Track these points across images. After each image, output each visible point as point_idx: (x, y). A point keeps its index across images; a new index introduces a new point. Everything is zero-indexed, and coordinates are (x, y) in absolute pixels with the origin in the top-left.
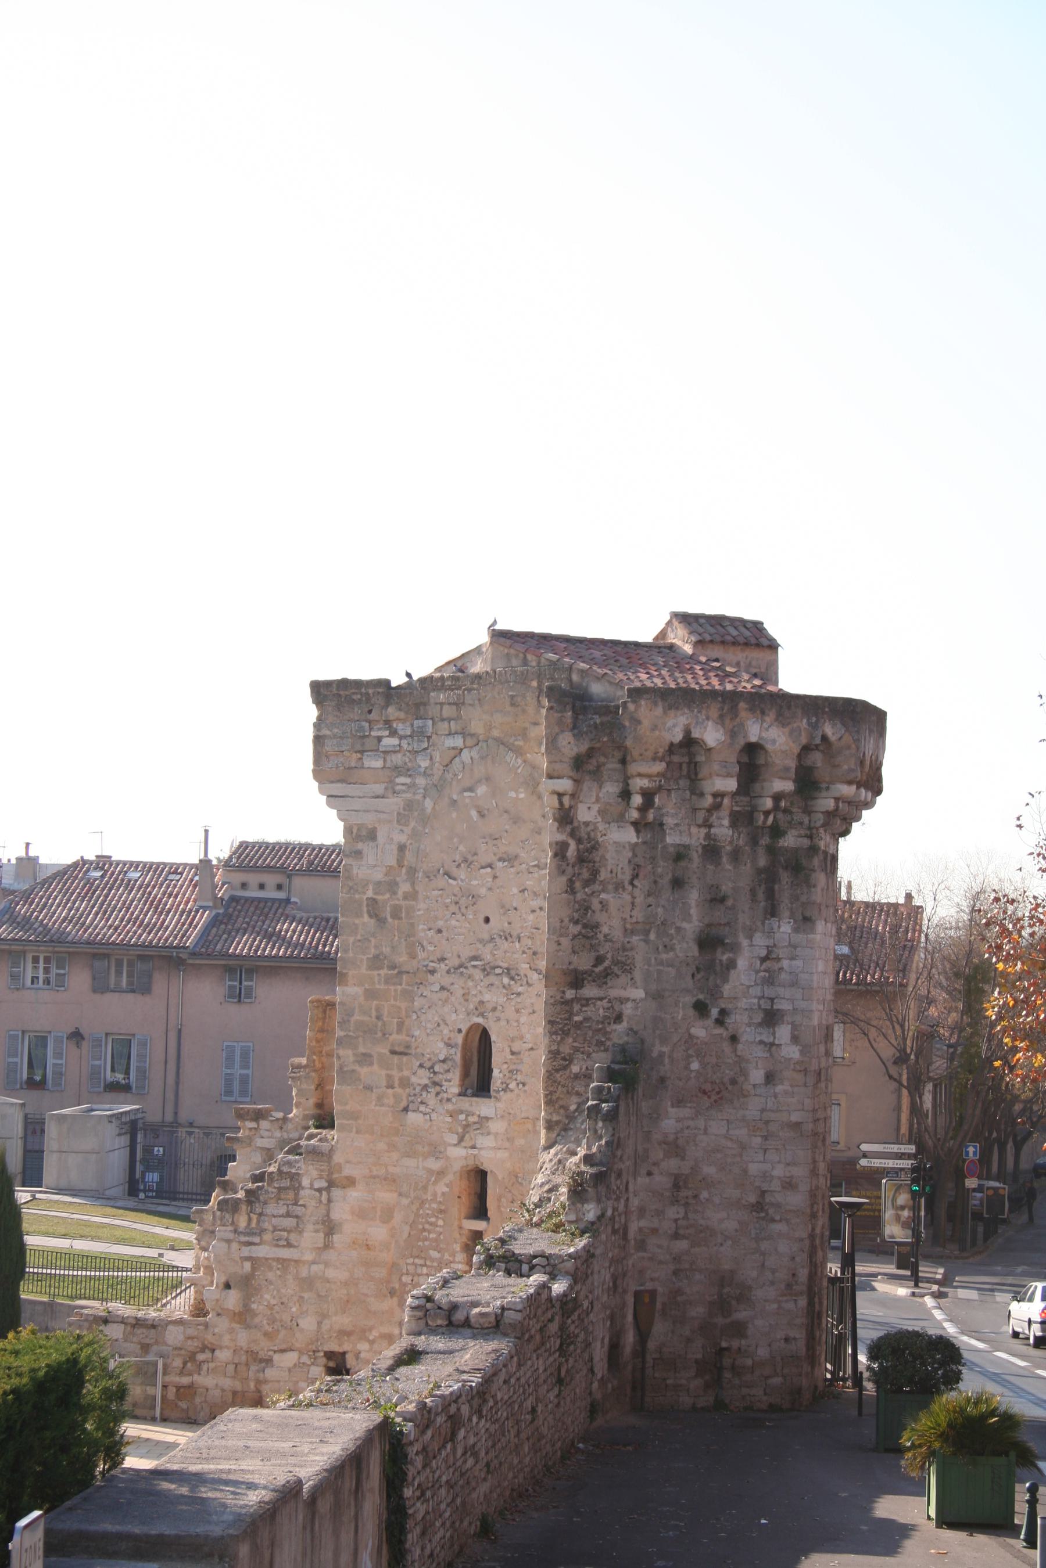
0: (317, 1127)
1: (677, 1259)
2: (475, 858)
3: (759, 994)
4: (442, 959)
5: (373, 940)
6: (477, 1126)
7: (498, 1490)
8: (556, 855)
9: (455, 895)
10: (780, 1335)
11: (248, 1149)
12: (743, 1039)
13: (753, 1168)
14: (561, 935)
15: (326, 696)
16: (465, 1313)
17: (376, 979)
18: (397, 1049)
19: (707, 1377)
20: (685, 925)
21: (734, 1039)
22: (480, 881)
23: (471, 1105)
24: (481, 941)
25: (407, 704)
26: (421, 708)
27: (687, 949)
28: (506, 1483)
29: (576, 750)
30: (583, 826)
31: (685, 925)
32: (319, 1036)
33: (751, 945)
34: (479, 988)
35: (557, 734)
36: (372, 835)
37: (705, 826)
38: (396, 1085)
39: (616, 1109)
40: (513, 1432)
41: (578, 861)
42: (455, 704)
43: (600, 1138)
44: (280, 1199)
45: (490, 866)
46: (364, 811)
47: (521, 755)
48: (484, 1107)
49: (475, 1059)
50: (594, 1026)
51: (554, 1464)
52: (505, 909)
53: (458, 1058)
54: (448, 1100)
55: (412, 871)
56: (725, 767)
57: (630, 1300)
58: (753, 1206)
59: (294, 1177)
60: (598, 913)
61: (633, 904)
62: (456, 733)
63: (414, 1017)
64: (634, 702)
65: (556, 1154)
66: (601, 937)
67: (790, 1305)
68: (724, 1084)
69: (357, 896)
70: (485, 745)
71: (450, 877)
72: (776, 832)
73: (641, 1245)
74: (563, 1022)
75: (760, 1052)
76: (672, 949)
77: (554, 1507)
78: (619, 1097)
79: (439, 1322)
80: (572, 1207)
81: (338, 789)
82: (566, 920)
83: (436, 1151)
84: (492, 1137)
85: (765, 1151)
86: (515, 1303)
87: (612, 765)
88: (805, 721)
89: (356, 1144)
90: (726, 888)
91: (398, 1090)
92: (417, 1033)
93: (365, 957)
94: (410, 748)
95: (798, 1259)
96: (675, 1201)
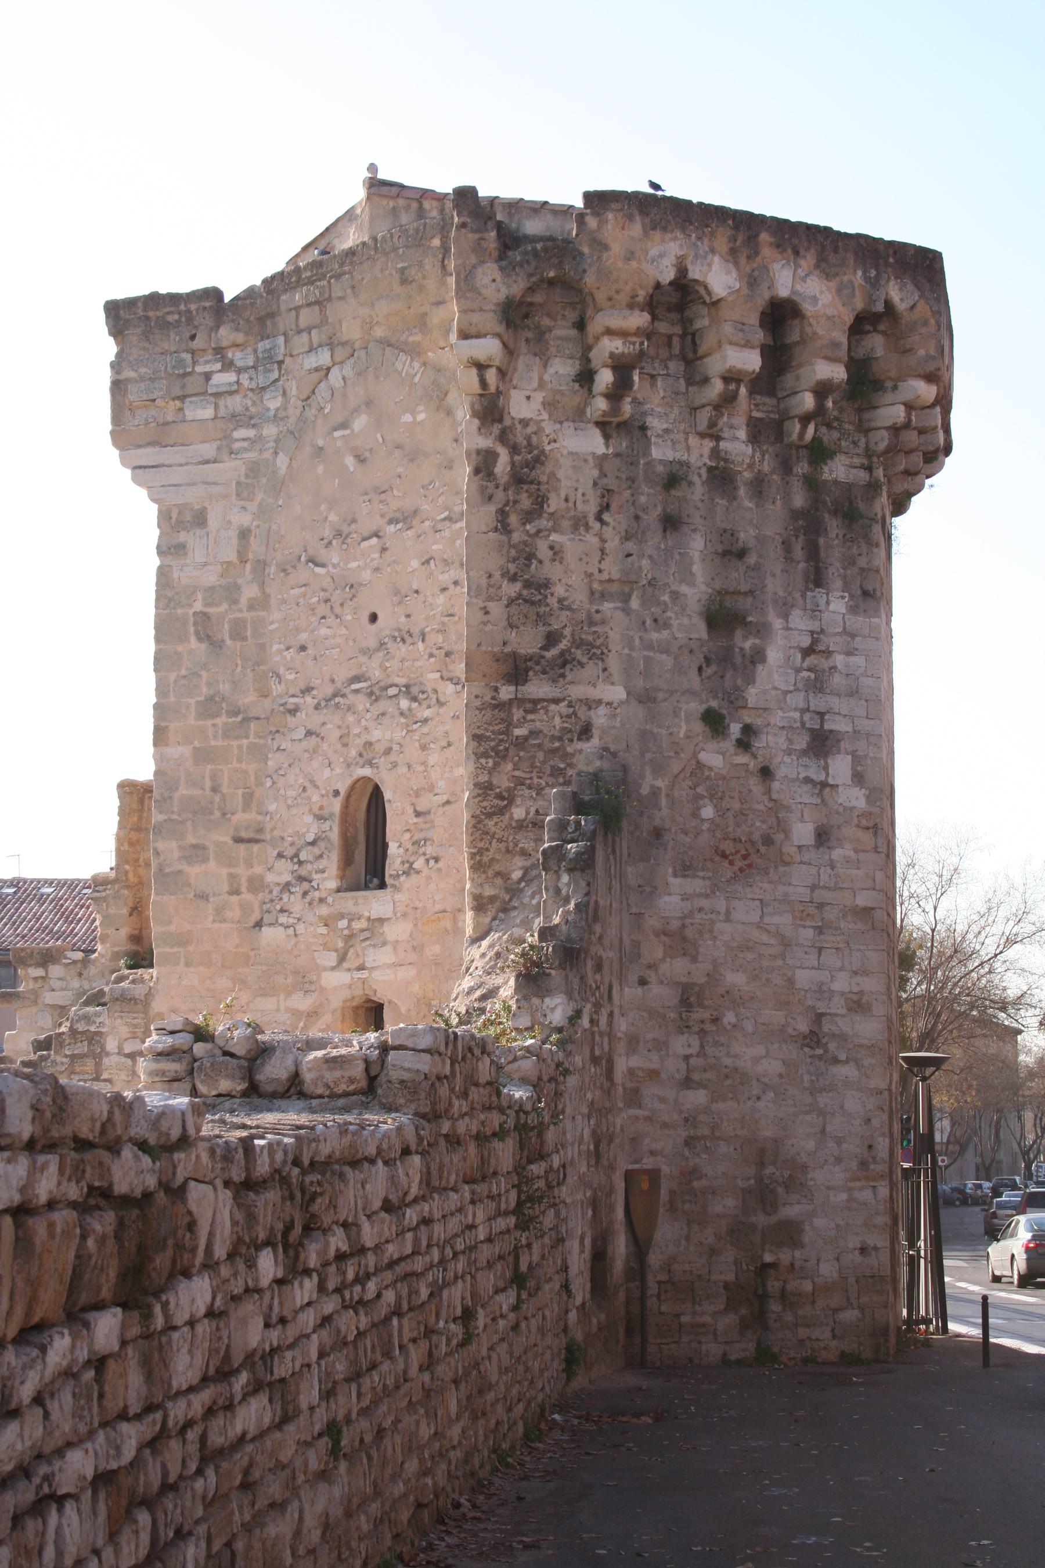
0: (130, 967)
1: (690, 1120)
2: (353, 526)
3: (802, 705)
4: (308, 690)
5: (204, 674)
6: (367, 934)
7: (374, 1507)
8: (477, 471)
9: (323, 590)
10: (853, 1242)
11: (34, 1009)
12: (781, 772)
13: (804, 978)
14: (489, 599)
15: (128, 321)
16: (289, 1062)
17: (210, 732)
18: (244, 834)
19: (743, 1311)
20: (684, 589)
21: (766, 773)
22: (360, 562)
23: (356, 904)
24: (364, 651)
25: (248, 321)
26: (268, 323)
27: (689, 626)
28: (400, 1488)
29: (504, 292)
30: (518, 426)
31: (684, 589)
32: (134, 836)
33: (788, 629)
34: (364, 723)
35: (474, 267)
36: (200, 520)
37: (711, 436)
38: (243, 889)
39: (591, 851)
40: (416, 1355)
41: (514, 481)
42: (318, 303)
43: (567, 901)
44: (73, 1073)
45: (376, 535)
46: (188, 484)
47: (419, 354)
48: (376, 904)
49: (362, 838)
50: (548, 745)
51: (513, 1447)
52: (400, 595)
53: (335, 835)
54: (321, 900)
55: (261, 565)
56: (742, 330)
57: (620, 1186)
58: (805, 1037)
59: (94, 1039)
60: (547, 563)
61: (602, 551)
62: (320, 346)
63: (269, 783)
64: (596, 214)
65: (491, 946)
66: (553, 601)
67: (867, 1195)
68: (753, 843)
69: (179, 611)
70: (363, 353)
71: (316, 565)
72: (819, 453)
73: (633, 1098)
74: (495, 740)
75: (805, 795)
76: (667, 625)
77: (527, 1547)
78: (594, 833)
79: (225, 1085)
80: (523, 1003)
81: (148, 455)
82: (497, 575)
83: (305, 981)
84: (389, 948)
85: (820, 950)
86: (414, 1034)
87: (562, 331)
88: (860, 273)
89: (185, 982)
90: (746, 536)
91: (247, 896)
92: (272, 807)
93: (192, 701)
94: (254, 385)
95: (875, 1122)
96: (684, 1027)
